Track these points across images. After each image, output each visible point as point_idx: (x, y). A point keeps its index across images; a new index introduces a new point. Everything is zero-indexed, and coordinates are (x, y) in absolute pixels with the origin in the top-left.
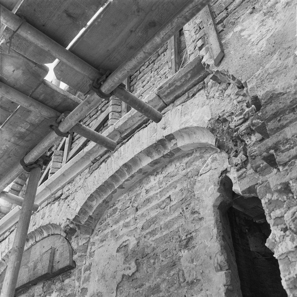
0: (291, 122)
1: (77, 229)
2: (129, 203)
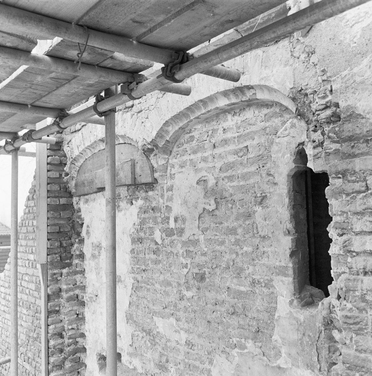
0: (362, 154)
1: (155, 149)
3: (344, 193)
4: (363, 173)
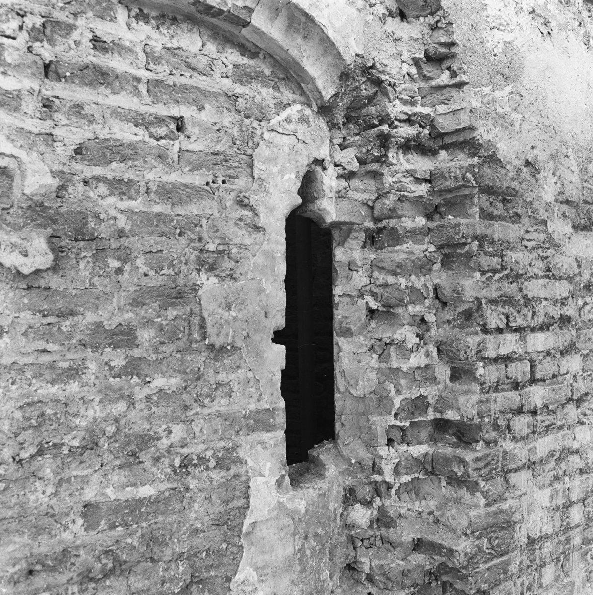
4: (501, 245)
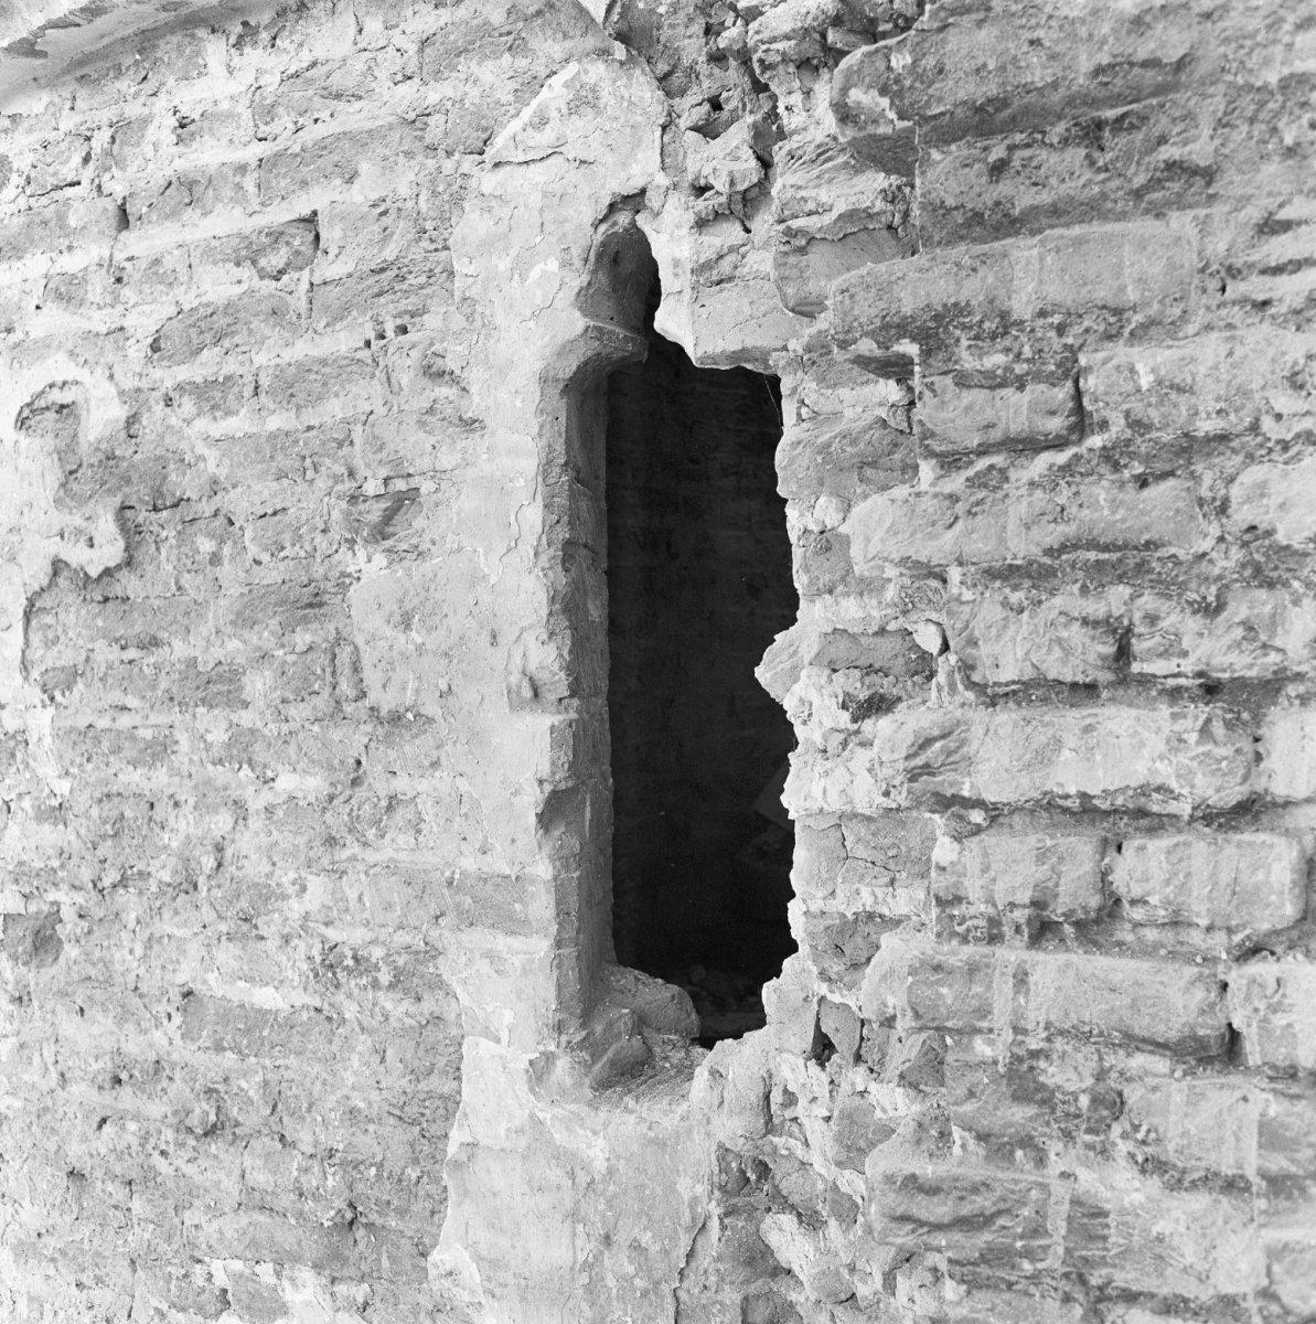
0: (1058, 213)
2: (77, 159)
3: (930, 454)
4: (1061, 330)
